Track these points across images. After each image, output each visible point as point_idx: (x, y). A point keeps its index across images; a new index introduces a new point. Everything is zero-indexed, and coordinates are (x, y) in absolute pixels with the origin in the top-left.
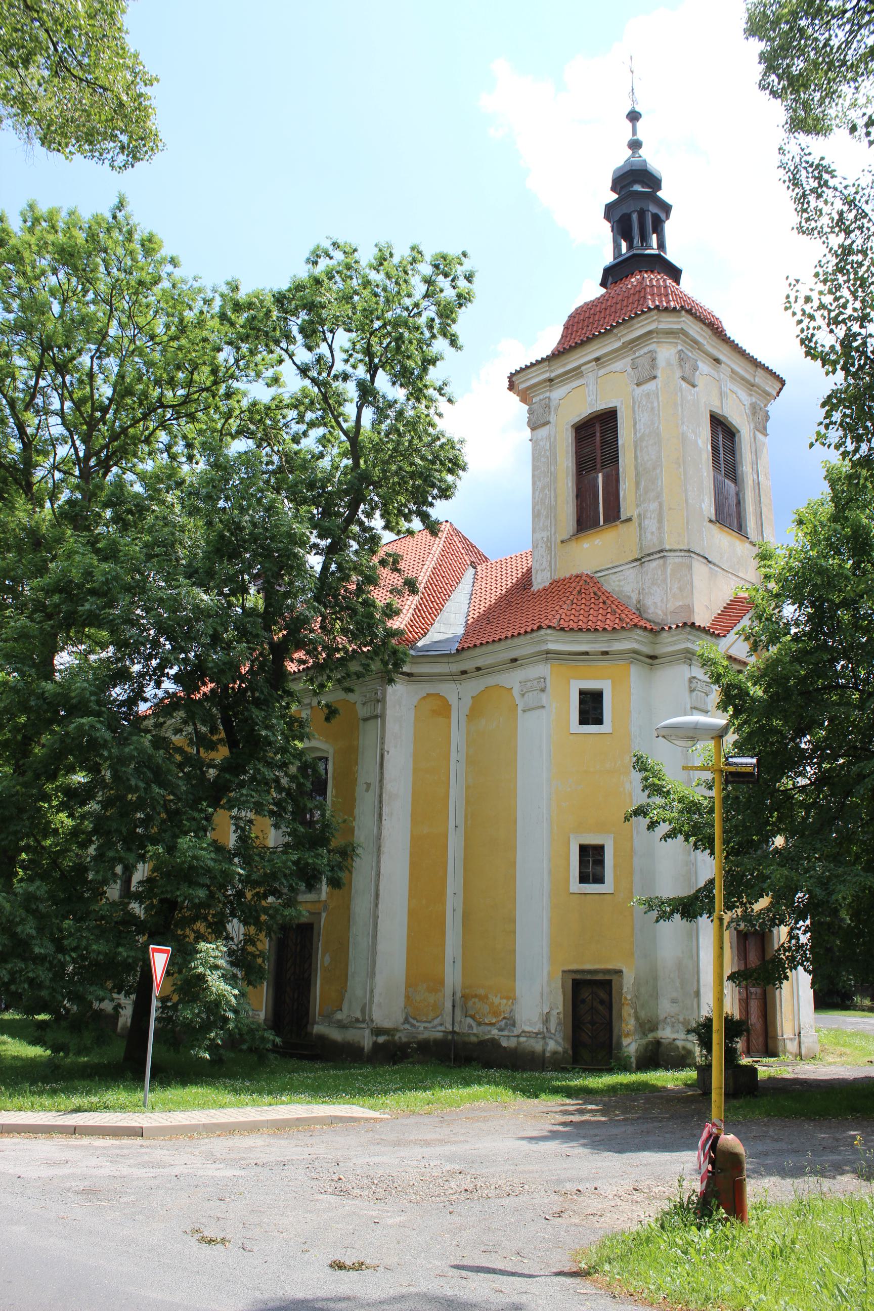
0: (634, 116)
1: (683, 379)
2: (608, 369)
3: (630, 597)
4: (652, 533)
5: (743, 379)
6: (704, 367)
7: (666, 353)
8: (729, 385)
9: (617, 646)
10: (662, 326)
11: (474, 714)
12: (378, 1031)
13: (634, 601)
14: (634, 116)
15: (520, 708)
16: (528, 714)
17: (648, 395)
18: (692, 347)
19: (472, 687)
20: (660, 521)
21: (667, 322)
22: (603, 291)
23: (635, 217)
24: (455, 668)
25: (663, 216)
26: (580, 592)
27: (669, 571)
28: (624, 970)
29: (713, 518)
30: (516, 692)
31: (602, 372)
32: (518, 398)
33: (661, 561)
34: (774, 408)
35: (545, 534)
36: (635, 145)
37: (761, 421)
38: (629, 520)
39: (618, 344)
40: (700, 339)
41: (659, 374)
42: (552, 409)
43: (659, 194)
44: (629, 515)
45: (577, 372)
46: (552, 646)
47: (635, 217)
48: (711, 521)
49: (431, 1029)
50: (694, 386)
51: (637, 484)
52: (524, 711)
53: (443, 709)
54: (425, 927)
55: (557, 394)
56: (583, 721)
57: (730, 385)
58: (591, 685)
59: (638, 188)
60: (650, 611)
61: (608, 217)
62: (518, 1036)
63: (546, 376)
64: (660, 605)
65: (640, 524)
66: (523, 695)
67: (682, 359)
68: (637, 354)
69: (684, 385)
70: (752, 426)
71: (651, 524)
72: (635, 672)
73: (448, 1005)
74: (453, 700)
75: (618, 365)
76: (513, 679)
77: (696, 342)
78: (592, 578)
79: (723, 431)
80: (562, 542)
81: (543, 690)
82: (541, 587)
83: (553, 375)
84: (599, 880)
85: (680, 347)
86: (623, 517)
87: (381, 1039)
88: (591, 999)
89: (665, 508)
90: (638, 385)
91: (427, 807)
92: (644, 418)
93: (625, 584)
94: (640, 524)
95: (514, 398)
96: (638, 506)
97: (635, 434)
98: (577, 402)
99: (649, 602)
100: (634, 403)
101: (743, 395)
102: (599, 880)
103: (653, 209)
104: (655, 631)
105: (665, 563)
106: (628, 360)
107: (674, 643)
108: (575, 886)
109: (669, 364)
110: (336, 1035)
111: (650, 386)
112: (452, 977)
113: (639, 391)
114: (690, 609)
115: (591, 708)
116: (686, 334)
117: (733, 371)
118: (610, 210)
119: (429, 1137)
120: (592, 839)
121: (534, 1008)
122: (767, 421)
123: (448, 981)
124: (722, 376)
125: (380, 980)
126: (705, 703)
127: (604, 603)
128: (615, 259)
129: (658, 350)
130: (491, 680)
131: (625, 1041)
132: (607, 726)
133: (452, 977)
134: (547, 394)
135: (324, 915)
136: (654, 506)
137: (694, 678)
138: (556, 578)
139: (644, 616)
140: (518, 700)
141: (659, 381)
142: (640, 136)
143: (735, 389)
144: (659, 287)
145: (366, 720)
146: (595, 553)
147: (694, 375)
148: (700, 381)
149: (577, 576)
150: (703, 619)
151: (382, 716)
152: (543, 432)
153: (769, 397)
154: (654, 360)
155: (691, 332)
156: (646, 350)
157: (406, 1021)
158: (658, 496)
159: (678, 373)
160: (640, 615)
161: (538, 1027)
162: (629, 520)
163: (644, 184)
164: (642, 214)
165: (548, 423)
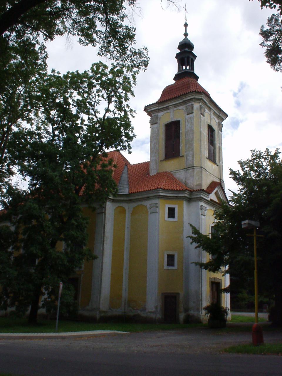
0: (186, 25)
1: (202, 114)
2: (178, 108)
3: (182, 180)
4: (190, 161)
5: (217, 114)
6: (207, 111)
7: (196, 105)
8: (213, 116)
9: (180, 195)
10: (196, 97)
11: (133, 214)
12: (101, 312)
13: (184, 181)
14: (186, 25)
15: (149, 213)
16: (151, 214)
17: (190, 118)
18: (204, 104)
19: (134, 205)
20: (193, 157)
21: (197, 96)
22: (174, 82)
23: (186, 59)
24: (128, 199)
25: (194, 59)
26: (167, 178)
27: (195, 173)
28: (180, 292)
29: (208, 157)
30: (148, 207)
31: (175, 109)
32: (147, 114)
33: (193, 170)
34: (224, 123)
35: (155, 158)
36: (186, 35)
37: (220, 126)
38: (183, 156)
39: (181, 101)
40: (207, 102)
41: (194, 112)
42: (158, 119)
43: (193, 51)
44: (183, 154)
45: (167, 108)
46: (161, 194)
47: (186, 59)
48: (207, 158)
49: (118, 312)
50: (204, 116)
51: (186, 145)
52: (151, 213)
53: (123, 211)
54: (116, 279)
55: (160, 114)
56: (169, 217)
57: (213, 116)
58: (172, 206)
59: (187, 49)
60: (189, 184)
61: (177, 57)
62: (147, 313)
63: (158, 108)
64: (193, 183)
65: (186, 158)
66: (150, 208)
67: (201, 108)
68: (187, 105)
69: (201, 116)
70: (218, 129)
71: (190, 158)
72: (185, 203)
73: (123, 303)
74: (126, 208)
75: (181, 107)
76: (148, 203)
77: (205, 102)
78: (170, 173)
79: (211, 129)
80: (161, 161)
81: (157, 207)
82: (153, 175)
83: (159, 108)
84: (173, 265)
85: (201, 104)
86: (181, 155)
87: (102, 315)
88: (170, 302)
89: (194, 153)
90: (188, 114)
91: (118, 241)
92: (189, 125)
93: (181, 175)
94: (186, 158)
95: (146, 114)
96: (186, 152)
97: (186, 130)
98: (167, 117)
99: (189, 182)
100: (186, 120)
101: (216, 119)
102: (173, 265)
103: (192, 57)
104: (191, 192)
105: (194, 171)
106: (185, 106)
107: (197, 195)
108: (166, 267)
109: (197, 109)
110: (86, 313)
111: (191, 115)
112: (125, 295)
113: (188, 116)
114: (201, 185)
115: (171, 213)
116: (203, 100)
117: (214, 112)
118: (178, 56)
119: (201, 309)
120: (171, 253)
121: (152, 303)
122: (222, 127)
123: (123, 296)
124: (211, 113)
125: (102, 296)
126: (205, 213)
127: (175, 181)
128: (178, 72)
129: (194, 104)
130: (139, 203)
131: (180, 315)
132: (176, 219)
133: (125, 295)
134: (157, 114)
135: (82, 275)
136: (191, 153)
137: (202, 206)
138: (158, 172)
139: (187, 186)
140: (149, 210)
141: (194, 114)
142: (188, 32)
143: (214, 117)
144: (194, 83)
145: (98, 213)
146: (171, 166)
147: (204, 113)
148: (206, 114)
149: (165, 172)
150: (205, 187)
151: (105, 213)
152: (155, 126)
153: (223, 120)
154: (193, 107)
155: (204, 100)
156: (191, 104)
157: (110, 309)
158: (193, 149)
159: (200, 113)
160: (186, 186)
161: (154, 310)
162: (183, 156)
163: (188, 48)
164: (188, 58)
165: (157, 123)
